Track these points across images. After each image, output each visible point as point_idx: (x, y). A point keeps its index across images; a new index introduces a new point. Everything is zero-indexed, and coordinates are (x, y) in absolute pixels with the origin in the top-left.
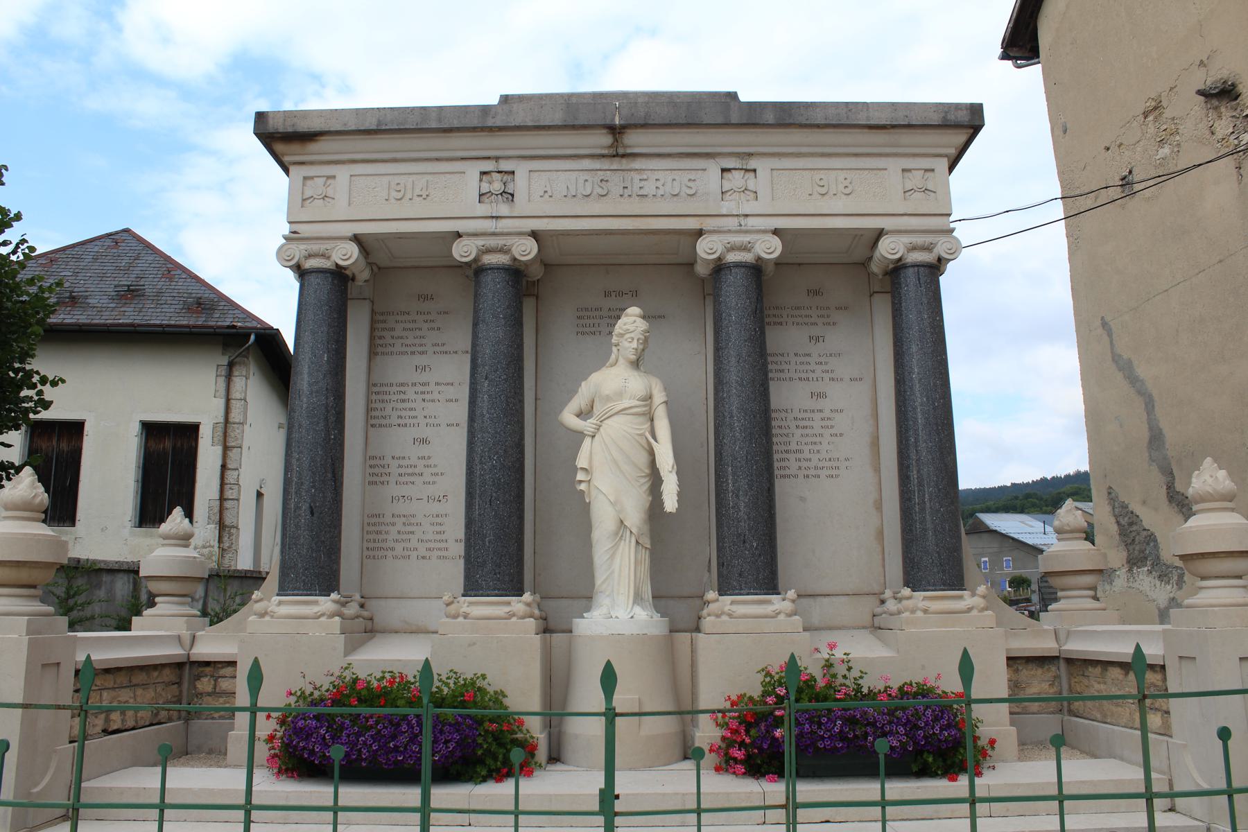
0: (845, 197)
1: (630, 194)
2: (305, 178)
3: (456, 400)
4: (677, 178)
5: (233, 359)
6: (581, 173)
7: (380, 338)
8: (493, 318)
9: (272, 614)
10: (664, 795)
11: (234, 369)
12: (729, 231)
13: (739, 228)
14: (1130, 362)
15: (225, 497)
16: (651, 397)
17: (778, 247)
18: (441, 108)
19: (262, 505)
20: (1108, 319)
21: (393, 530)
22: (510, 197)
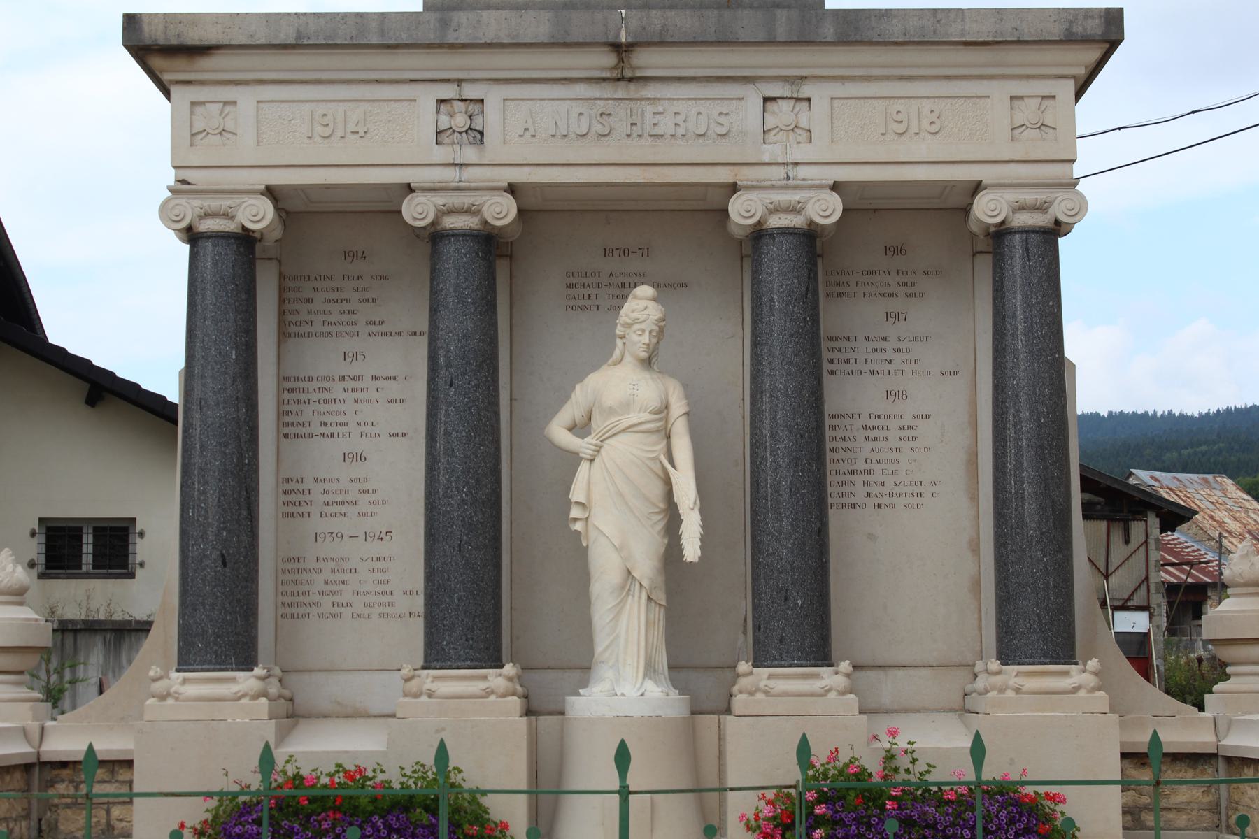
0: (930, 137)
1: (640, 133)
2: (193, 104)
3: (402, 401)
4: (702, 110)
6: (574, 103)
7: (292, 312)
8: (459, 303)
9: (177, 695)
12: (773, 187)
13: (785, 182)
16: (667, 407)
17: (837, 208)
18: (383, 16)
21: (318, 579)
22: (479, 136)
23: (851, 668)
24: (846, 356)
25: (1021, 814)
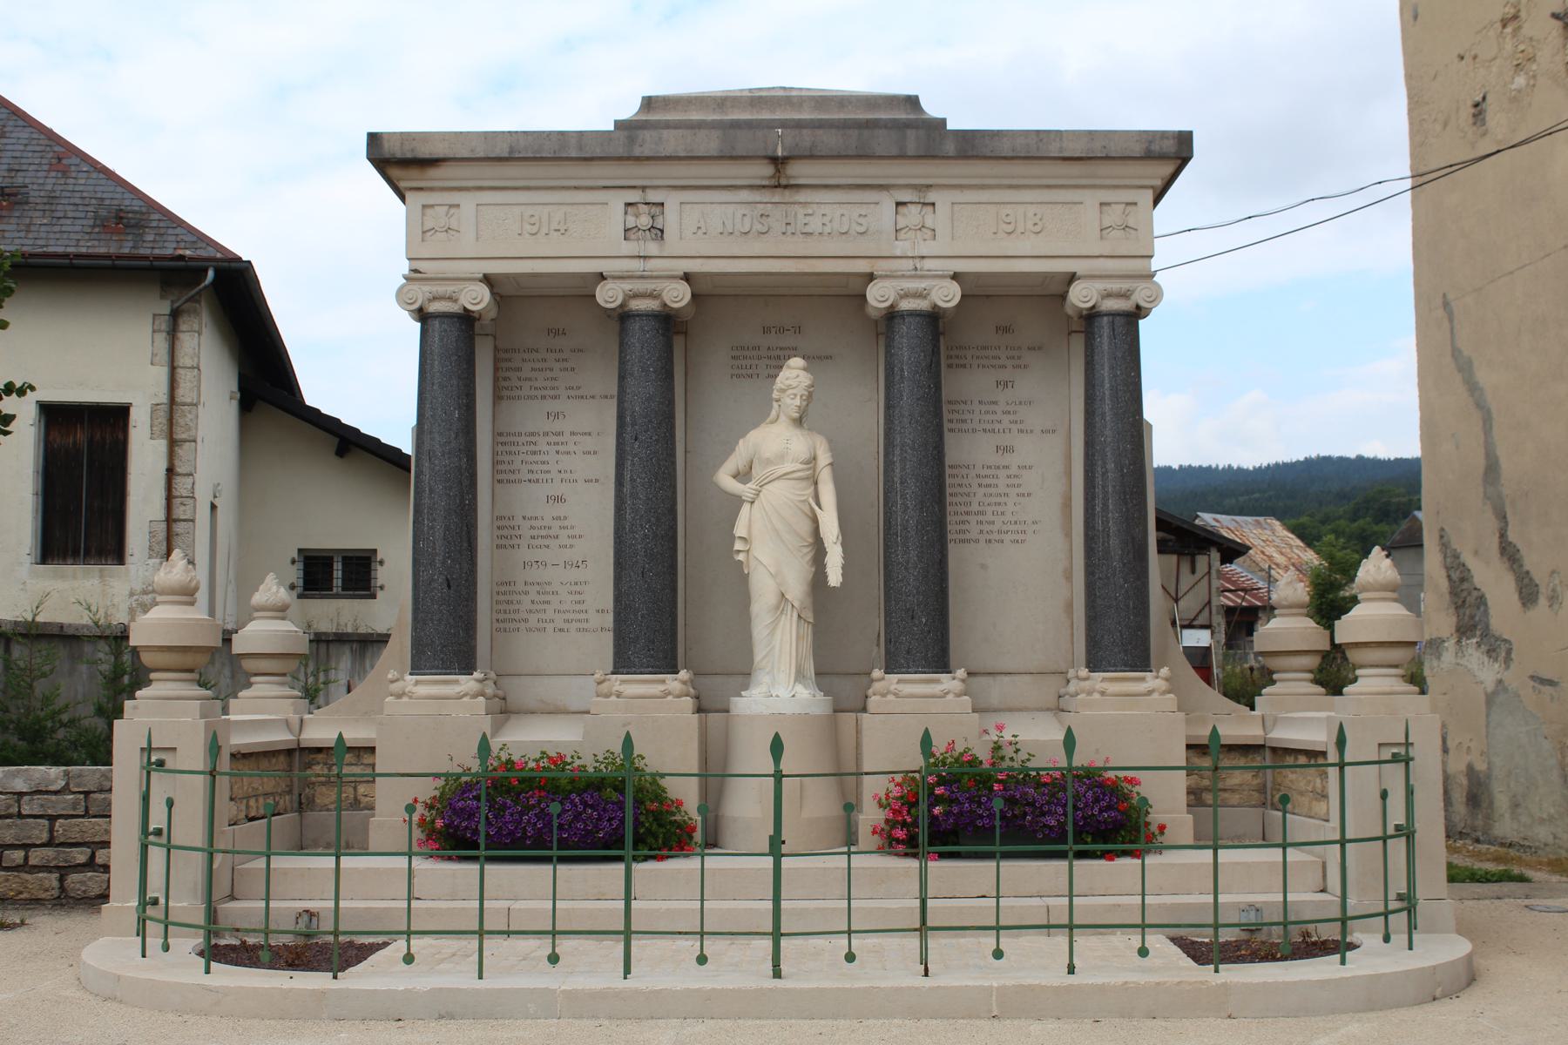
2: (424, 206)
3: (595, 453)
5: (178, 307)
7: (505, 379)
8: (642, 371)
10: (825, 869)
11: (181, 321)
14: (1470, 362)
15: (174, 517)
16: (815, 458)
19: (216, 522)
20: (1450, 297)
21: (526, 600)
22: (659, 233)
23: (966, 675)
24: (964, 417)
25: (1104, 795)
